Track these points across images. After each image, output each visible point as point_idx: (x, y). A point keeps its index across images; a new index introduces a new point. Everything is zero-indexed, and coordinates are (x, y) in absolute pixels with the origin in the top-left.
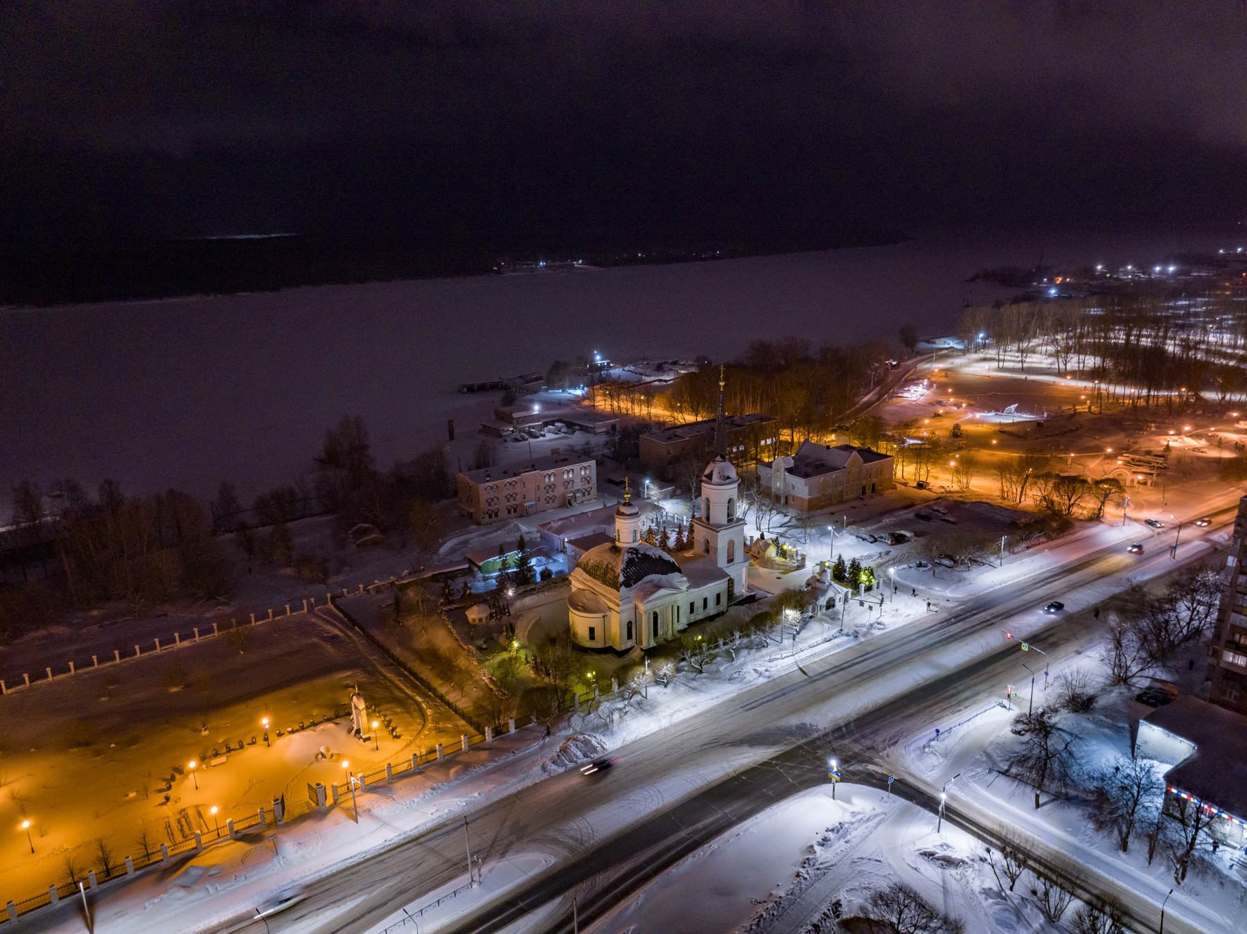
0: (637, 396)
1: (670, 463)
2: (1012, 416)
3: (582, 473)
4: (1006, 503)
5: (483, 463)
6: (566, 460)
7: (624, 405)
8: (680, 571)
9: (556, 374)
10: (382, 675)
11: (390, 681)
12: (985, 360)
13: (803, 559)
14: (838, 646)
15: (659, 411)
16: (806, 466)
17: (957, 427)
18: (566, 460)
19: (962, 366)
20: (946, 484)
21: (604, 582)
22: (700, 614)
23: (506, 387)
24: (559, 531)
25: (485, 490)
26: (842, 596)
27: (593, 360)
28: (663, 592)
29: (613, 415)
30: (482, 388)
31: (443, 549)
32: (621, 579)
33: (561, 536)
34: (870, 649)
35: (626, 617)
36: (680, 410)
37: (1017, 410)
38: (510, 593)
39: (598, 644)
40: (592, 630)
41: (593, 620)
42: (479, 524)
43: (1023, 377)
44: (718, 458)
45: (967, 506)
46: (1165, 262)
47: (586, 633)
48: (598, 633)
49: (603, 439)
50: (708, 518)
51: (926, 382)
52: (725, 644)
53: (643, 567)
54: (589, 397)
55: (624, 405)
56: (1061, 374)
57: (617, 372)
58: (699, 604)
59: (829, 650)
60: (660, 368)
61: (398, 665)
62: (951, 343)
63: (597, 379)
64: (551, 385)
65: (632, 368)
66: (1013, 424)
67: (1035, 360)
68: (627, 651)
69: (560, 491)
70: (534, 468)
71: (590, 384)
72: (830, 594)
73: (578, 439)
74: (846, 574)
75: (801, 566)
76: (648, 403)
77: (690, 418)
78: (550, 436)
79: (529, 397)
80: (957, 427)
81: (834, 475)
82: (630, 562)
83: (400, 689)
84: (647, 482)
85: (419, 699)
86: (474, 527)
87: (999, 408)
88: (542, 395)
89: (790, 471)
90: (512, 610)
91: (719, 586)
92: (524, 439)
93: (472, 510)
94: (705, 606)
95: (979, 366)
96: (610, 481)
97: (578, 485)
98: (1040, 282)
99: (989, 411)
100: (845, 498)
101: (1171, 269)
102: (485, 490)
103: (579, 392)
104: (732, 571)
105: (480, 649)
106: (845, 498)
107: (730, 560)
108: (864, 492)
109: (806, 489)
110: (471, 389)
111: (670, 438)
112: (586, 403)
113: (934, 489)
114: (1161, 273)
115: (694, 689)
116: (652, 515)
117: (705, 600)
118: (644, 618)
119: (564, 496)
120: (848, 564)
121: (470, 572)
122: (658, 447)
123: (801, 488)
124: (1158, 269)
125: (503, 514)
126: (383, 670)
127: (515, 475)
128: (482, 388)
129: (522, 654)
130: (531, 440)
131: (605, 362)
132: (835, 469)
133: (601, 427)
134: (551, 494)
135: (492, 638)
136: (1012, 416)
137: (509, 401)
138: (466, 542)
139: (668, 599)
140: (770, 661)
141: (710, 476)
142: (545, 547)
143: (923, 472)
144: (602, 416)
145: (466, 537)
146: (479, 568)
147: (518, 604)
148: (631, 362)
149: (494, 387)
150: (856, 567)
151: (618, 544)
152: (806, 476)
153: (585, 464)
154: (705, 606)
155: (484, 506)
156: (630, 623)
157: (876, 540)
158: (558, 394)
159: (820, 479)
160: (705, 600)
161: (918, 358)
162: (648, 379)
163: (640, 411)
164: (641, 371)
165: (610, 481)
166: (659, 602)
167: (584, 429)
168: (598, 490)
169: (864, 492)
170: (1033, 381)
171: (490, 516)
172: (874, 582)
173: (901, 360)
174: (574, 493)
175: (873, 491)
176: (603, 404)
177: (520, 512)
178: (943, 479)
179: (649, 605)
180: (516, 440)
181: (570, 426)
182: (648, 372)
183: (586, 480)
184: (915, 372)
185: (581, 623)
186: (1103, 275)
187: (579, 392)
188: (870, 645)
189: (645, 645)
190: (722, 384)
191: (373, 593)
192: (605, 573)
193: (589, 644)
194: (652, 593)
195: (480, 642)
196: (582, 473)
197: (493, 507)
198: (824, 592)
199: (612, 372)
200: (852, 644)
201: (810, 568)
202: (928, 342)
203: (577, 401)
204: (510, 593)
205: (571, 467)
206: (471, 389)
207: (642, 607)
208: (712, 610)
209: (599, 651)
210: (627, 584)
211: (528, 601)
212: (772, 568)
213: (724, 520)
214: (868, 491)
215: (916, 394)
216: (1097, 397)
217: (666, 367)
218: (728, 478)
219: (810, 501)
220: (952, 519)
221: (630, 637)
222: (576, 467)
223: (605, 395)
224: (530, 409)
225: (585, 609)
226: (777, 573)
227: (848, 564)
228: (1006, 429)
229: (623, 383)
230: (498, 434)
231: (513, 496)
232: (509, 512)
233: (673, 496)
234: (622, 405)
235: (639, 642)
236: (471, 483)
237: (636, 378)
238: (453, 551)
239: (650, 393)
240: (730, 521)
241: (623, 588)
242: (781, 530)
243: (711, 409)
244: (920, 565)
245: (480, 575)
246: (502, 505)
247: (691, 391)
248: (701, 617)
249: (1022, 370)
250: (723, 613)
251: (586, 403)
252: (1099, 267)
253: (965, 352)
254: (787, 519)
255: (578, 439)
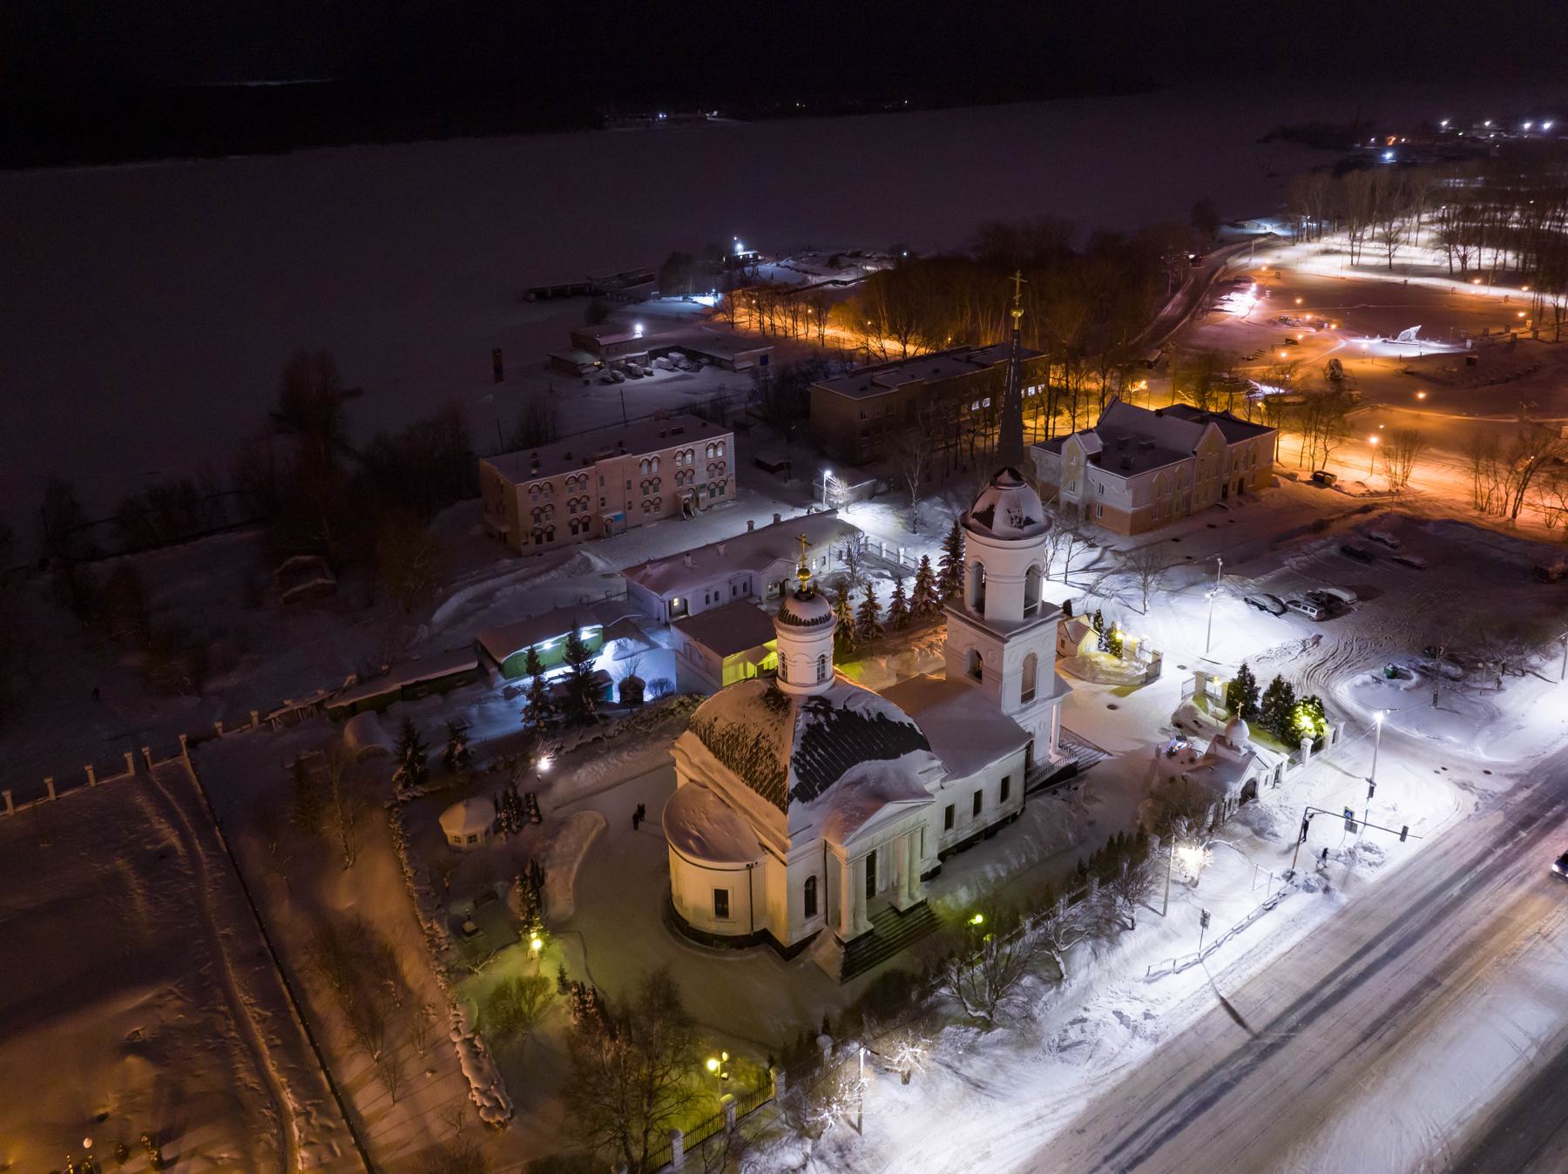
0: (802, 307)
1: (865, 433)
2: (1412, 346)
3: (713, 453)
4: (1490, 520)
5: (537, 437)
6: (679, 431)
7: (781, 321)
8: (927, 747)
9: (676, 272)
10: (231, 1001)
11: (242, 1025)
12: (1327, 252)
13: (1157, 662)
14: (1295, 922)
15: (838, 333)
16: (1124, 446)
17: (1335, 365)
18: (679, 431)
19: (1298, 261)
20: (1363, 476)
21: (751, 782)
22: (966, 829)
23: (597, 293)
24: (662, 586)
25: (527, 494)
26: (1271, 773)
27: (733, 251)
28: (890, 808)
29: (766, 338)
30: (560, 294)
31: (440, 615)
32: (792, 781)
33: (666, 596)
34: (1371, 929)
35: (801, 871)
36: (876, 330)
37: (1420, 336)
38: (544, 764)
39: (736, 926)
40: (721, 896)
41: (728, 876)
42: (517, 554)
43: (1399, 279)
44: (1006, 477)
45: (1430, 529)
46: (1538, 117)
47: (708, 902)
48: (736, 903)
49: (747, 383)
50: (980, 605)
51: (1254, 287)
52: (1035, 925)
53: (840, 748)
54: (726, 308)
55: (781, 321)
56: (1466, 275)
57: (768, 268)
58: (965, 806)
59: (1277, 936)
60: (834, 264)
61: (268, 956)
62: (1268, 227)
63: (736, 280)
64: (667, 289)
65: (791, 263)
66: (1421, 359)
67: (1410, 254)
68: (804, 944)
69: (668, 488)
70: (621, 448)
71: (726, 289)
72: (1250, 773)
73: (705, 382)
74: (1268, 710)
75: (1152, 676)
76: (821, 320)
77: (892, 346)
78: (660, 375)
79: (631, 308)
80: (1335, 365)
81: (1176, 467)
82: (812, 736)
83: (255, 1054)
84: (828, 474)
85: (290, 1101)
86: (507, 562)
87: (1390, 331)
88: (653, 305)
89: (1096, 459)
90: (544, 803)
91: (1009, 763)
92: (618, 380)
93: (504, 530)
94: (977, 808)
95: (1328, 259)
96: (759, 464)
97: (702, 477)
98: (1366, 142)
99: (1373, 336)
100: (1194, 507)
101: (1547, 126)
102: (527, 494)
103: (709, 301)
104: (1029, 721)
105: (457, 929)
106: (1194, 507)
107: (1028, 696)
108: (1225, 495)
109: (1129, 495)
110: (542, 295)
111: (863, 389)
112: (721, 317)
113: (1347, 487)
114: (1530, 131)
115: (977, 1086)
116: (840, 545)
117: (978, 795)
118: (846, 875)
119: (676, 498)
120: (1263, 686)
121: (481, 676)
122: (842, 404)
123: (1117, 491)
124: (1527, 126)
125: (562, 534)
126: (233, 975)
127: (586, 463)
128: (560, 294)
129: (549, 971)
130: (629, 382)
131: (750, 254)
132: (1175, 456)
133: (745, 360)
134: (652, 496)
135: (491, 895)
136: (1412, 346)
137: (598, 317)
138: (489, 595)
139: (900, 824)
140: (1151, 979)
141: (987, 517)
142: (634, 616)
143: (1320, 453)
144: (745, 341)
145: (490, 583)
146: (501, 668)
147: (561, 787)
148: (789, 253)
149: (579, 292)
150: (1280, 690)
151: (782, 686)
152: (1125, 469)
153: (715, 440)
154: (977, 808)
155: (528, 524)
156: (811, 882)
157: (1285, 610)
158: (677, 303)
159: (1153, 476)
160: (978, 795)
161: (1226, 249)
162: (815, 280)
163: (807, 331)
164: (804, 266)
165: (759, 464)
166: (879, 835)
167: (715, 363)
168: (740, 481)
169: (1225, 495)
170: (1417, 287)
171: (539, 540)
172: (1328, 731)
173: (1202, 252)
174: (696, 492)
175: (1241, 491)
176: (746, 319)
177: (595, 531)
178: (1360, 468)
179: (856, 846)
180: (605, 381)
181: (694, 357)
182: (815, 268)
183: (717, 466)
184: (1227, 272)
185: (694, 883)
186: (1451, 134)
187: (709, 301)
188: (1365, 915)
189: (846, 931)
190: (1017, 314)
191: (278, 728)
192: (753, 760)
193: (715, 926)
194: (866, 814)
195: (464, 908)
196: (713, 453)
197: (545, 523)
198: (1240, 769)
199: (761, 268)
200: (1323, 916)
201: (1171, 690)
202: (1234, 225)
203: (707, 313)
204: (544, 764)
205: (690, 446)
206: (542, 295)
207: (841, 851)
208: (990, 816)
209: (738, 943)
210: (805, 793)
211: (584, 776)
212: (1094, 680)
213: (1017, 614)
214: (1232, 493)
215: (1242, 306)
216: (1538, 312)
217: (844, 261)
218: (1029, 521)
219: (1135, 515)
220: (1417, 561)
221: (810, 909)
222: (698, 446)
223: (749, 306)
224: (628, 329)
225: (706, 850)
226: (1105, 693)
227: (1263, 686)
228: (1417, 368)
229: (778, 287)
230: (575, 371)
231: (582, 503)
232: (575, 531)
233: (871, 496)
234: (778, 322)
235: (834, 920)
236: (503, 480)
237: (799, 277)
238: (460, 616)
239: (822, 304)
240: (1029, 613)
241: (795, 806)
242: (1089, 578)
243: (928, 338)
244: (1394, 674)
245: (501, 681)
246: (561, 520)
247: (889, 302)
248: (968, 833)
249: (1390, 269)
250: (1014, 817)
251: (721, 317)
252: (1444, 123)
253: (1294, 240)
254: (1095, 554)
255: (705, 382)
